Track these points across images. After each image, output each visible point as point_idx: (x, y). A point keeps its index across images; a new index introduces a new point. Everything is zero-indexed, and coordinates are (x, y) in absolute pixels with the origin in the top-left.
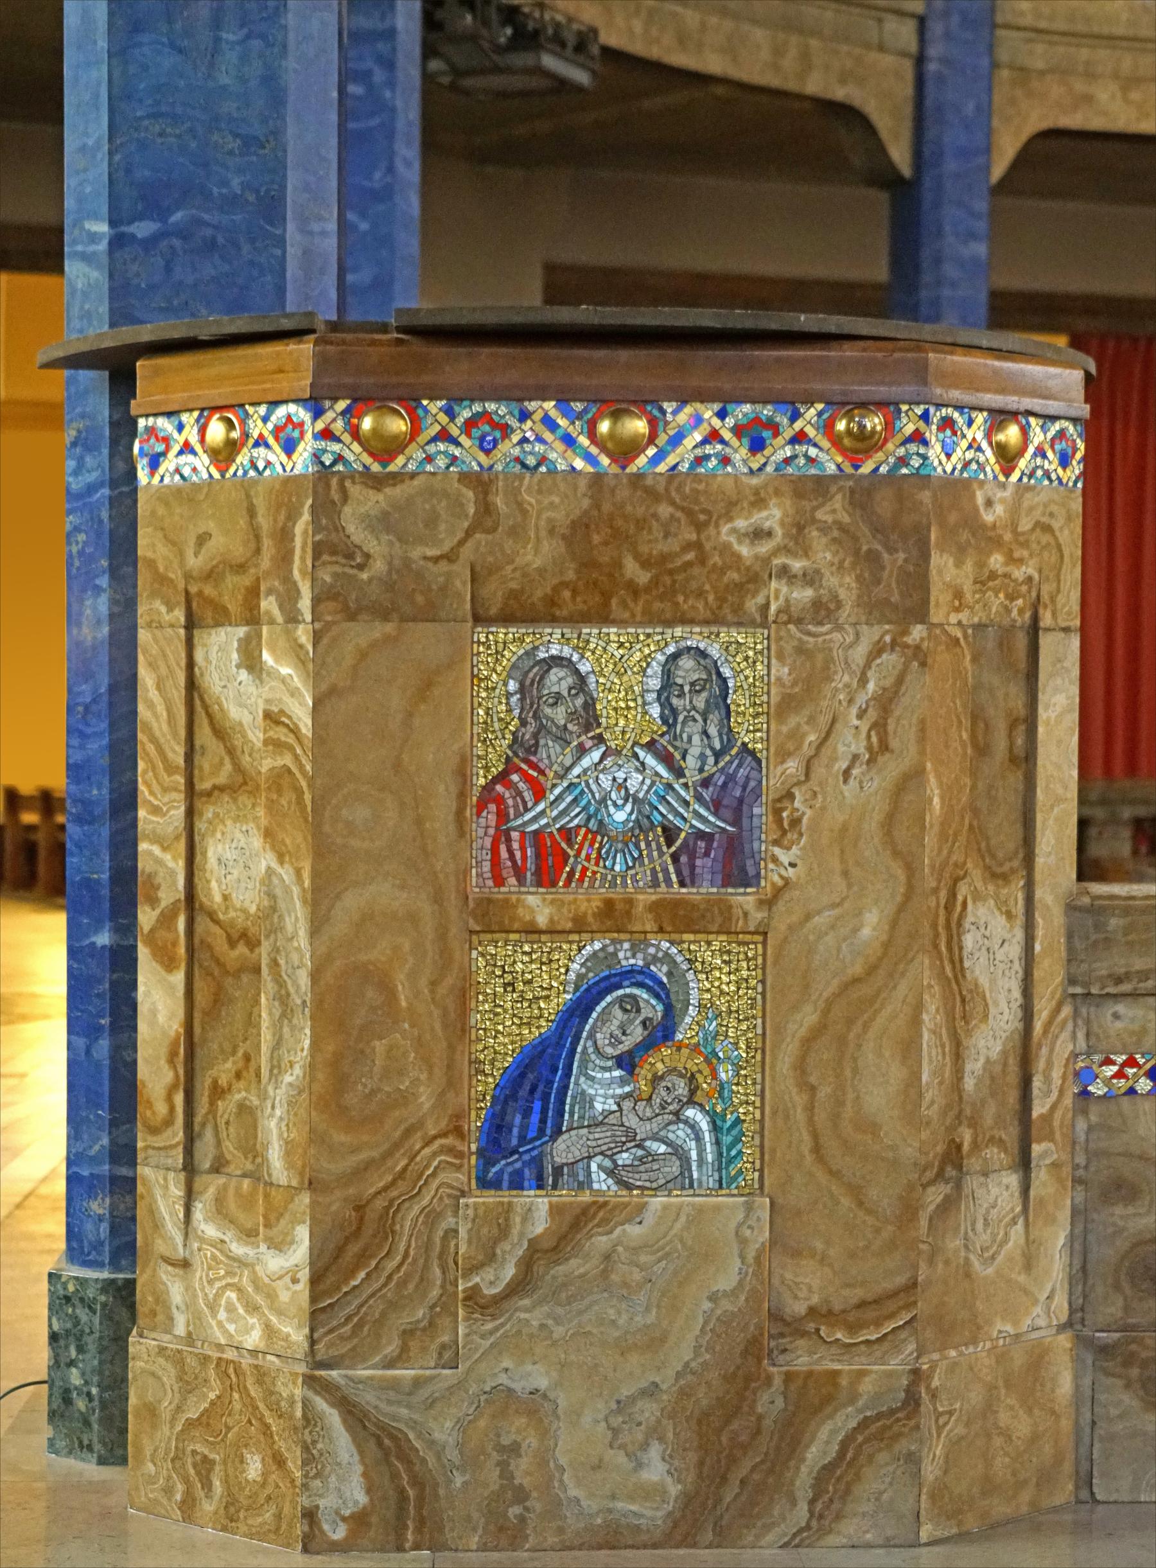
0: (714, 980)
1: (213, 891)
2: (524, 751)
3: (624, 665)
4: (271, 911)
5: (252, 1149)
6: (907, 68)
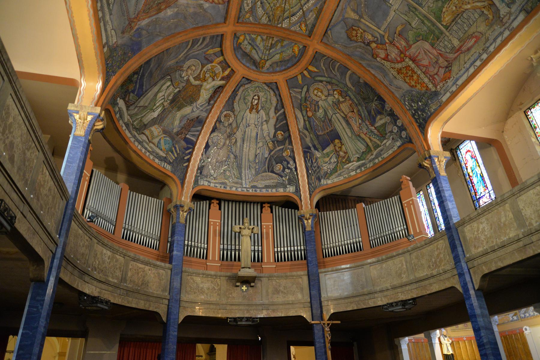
6: (166, 307)
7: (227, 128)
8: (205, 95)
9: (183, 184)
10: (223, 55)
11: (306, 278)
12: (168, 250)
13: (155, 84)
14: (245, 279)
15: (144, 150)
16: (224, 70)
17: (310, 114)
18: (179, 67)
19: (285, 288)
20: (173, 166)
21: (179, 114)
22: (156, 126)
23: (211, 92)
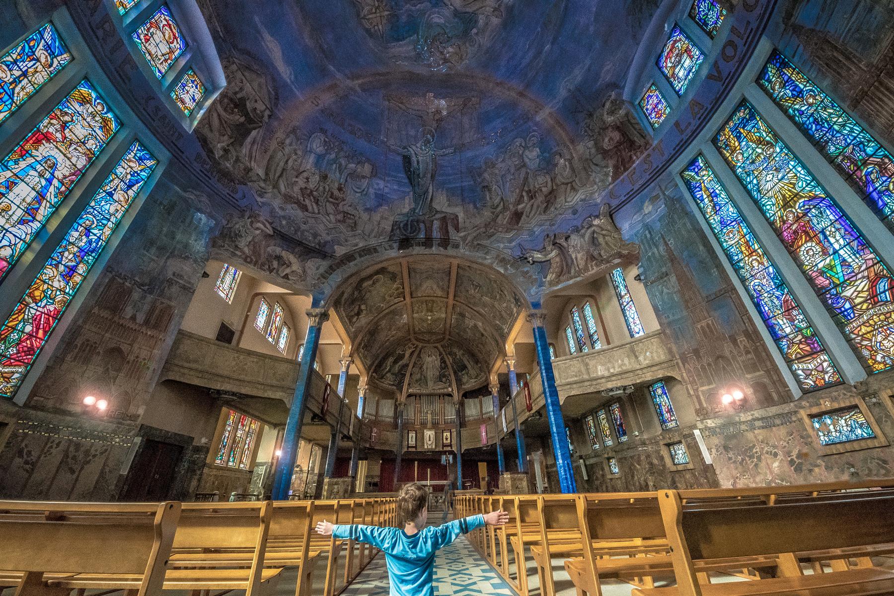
3: (336, 487)
8: (407, 355)
14: (59, 515)
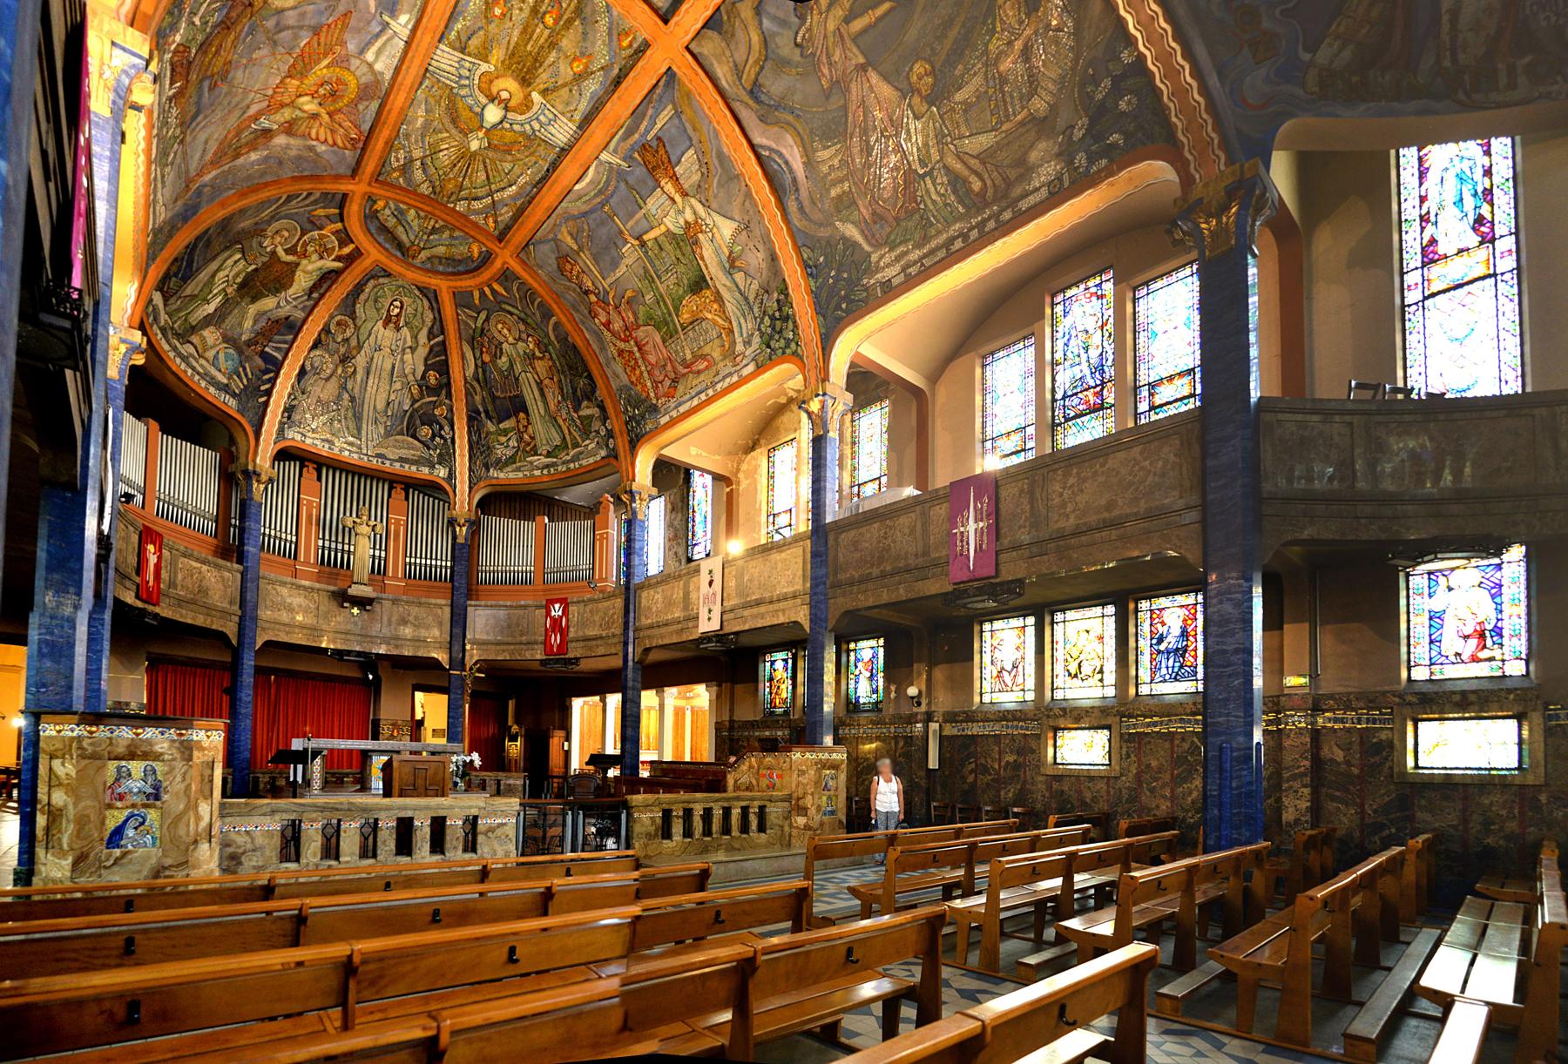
0: (152, 815)
1: (54, 802)
2: (117, 780)
3: (137, 767)
4: (66, 806)
5: (61, 845)
7: (341, 349)
8: (302, 281)
9: (258, 434)
10: (342, 220)
11: (447, 610)
12: (233, 538)
13: (214, 258)
15: (190, 372)
16: (342, 244)
17: (487, 358)
18: (258, 231)
19: (416, 618)
20: (240, 401)
21: (253, 309)
22: (212, 328)
23: (315, 277)
